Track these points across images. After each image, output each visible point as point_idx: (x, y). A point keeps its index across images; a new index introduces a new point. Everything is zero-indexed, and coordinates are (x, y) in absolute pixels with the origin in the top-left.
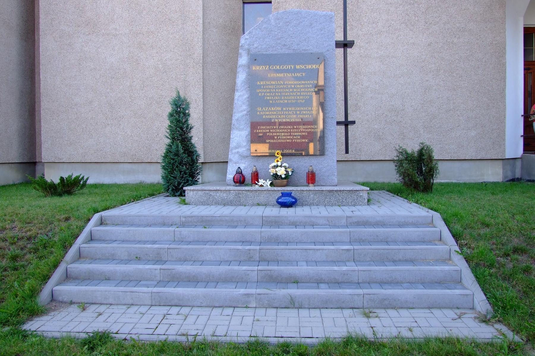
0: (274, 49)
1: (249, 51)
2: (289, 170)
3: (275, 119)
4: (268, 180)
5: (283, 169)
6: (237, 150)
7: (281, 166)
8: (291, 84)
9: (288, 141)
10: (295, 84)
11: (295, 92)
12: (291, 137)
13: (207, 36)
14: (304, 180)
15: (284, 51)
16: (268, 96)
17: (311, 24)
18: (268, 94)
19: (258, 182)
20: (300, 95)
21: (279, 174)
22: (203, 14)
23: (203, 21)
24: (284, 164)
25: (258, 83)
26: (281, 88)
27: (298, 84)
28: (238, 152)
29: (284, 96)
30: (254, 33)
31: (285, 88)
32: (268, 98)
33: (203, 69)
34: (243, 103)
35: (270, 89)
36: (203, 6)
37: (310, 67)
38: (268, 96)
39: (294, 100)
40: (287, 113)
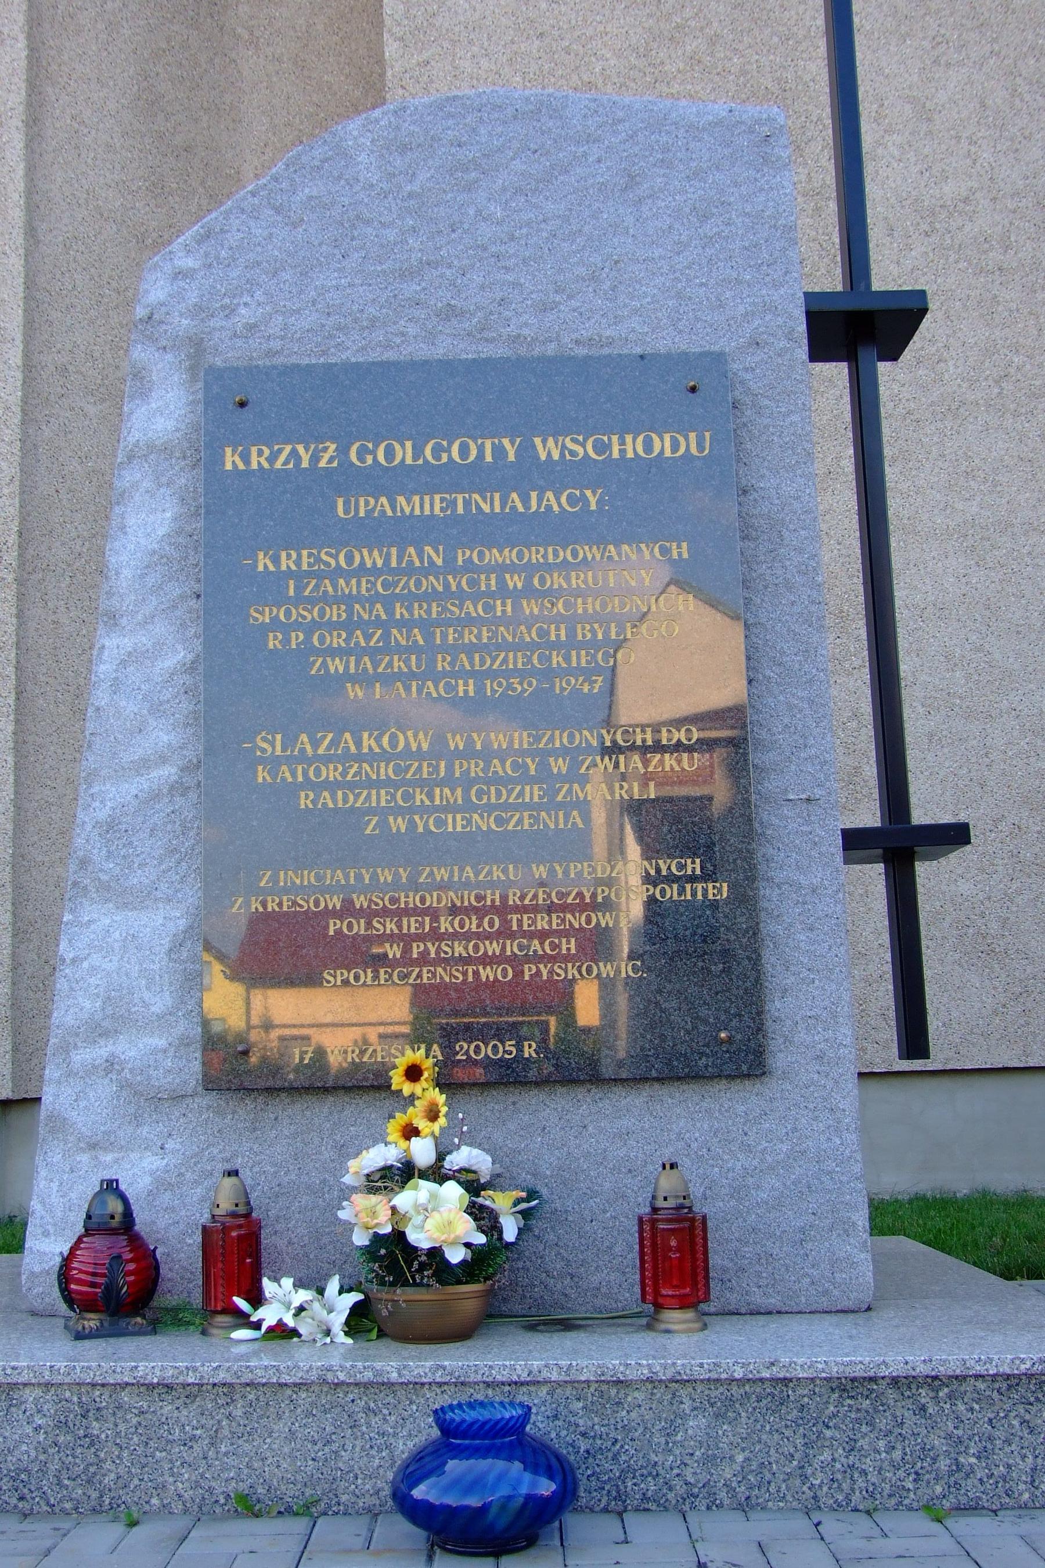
0: (379, 336)
1: (196, 348)
2: (501, 1202)
3: (383, 813)
4: (333, 1286)
5: (453, 1191)
6: (103, 1051)
7: (437, 1174)
8: (502, 569)
9: (486, 973)
10: (530, 569)
11: (533, 620)
12: (512, 948)
13: (47, 432)
14: (618, 1272)
15: (448, 345)
16: (334, 652)
17: (632, 180)
18: (337, 640)
19: (257, 1299)
20: (572, 644)
21: (420, 1238)
22: (30, 326)
23: (27, 355)
24: (461, 1157)
25: (263, 562)
26: (432, 596)
27: (549, 568)
28: (111, 1064)
29: (454, 650)
30: (233, 238)
31: (461, 596)
32: (336, 665)
33: (21, 597)
34: (157, 710)
35: (349, 600)
36: (30, 284)
37: (633, 446)
38: (334, 652)
39: (522, 675)
40: (475, 769)
